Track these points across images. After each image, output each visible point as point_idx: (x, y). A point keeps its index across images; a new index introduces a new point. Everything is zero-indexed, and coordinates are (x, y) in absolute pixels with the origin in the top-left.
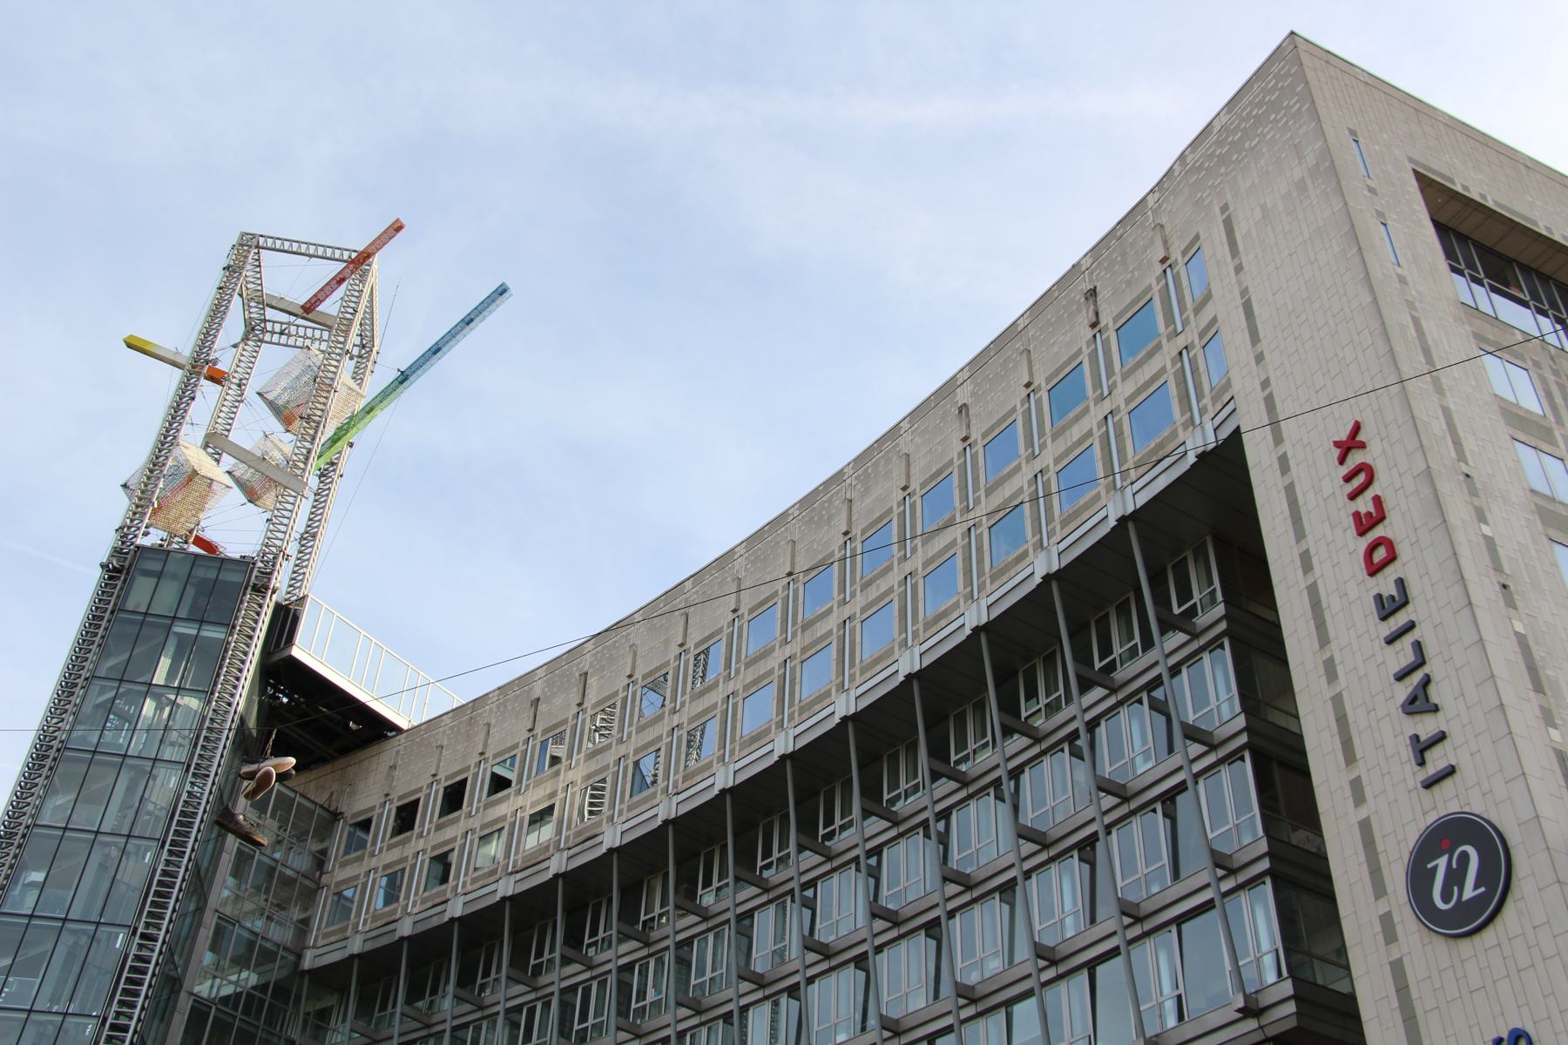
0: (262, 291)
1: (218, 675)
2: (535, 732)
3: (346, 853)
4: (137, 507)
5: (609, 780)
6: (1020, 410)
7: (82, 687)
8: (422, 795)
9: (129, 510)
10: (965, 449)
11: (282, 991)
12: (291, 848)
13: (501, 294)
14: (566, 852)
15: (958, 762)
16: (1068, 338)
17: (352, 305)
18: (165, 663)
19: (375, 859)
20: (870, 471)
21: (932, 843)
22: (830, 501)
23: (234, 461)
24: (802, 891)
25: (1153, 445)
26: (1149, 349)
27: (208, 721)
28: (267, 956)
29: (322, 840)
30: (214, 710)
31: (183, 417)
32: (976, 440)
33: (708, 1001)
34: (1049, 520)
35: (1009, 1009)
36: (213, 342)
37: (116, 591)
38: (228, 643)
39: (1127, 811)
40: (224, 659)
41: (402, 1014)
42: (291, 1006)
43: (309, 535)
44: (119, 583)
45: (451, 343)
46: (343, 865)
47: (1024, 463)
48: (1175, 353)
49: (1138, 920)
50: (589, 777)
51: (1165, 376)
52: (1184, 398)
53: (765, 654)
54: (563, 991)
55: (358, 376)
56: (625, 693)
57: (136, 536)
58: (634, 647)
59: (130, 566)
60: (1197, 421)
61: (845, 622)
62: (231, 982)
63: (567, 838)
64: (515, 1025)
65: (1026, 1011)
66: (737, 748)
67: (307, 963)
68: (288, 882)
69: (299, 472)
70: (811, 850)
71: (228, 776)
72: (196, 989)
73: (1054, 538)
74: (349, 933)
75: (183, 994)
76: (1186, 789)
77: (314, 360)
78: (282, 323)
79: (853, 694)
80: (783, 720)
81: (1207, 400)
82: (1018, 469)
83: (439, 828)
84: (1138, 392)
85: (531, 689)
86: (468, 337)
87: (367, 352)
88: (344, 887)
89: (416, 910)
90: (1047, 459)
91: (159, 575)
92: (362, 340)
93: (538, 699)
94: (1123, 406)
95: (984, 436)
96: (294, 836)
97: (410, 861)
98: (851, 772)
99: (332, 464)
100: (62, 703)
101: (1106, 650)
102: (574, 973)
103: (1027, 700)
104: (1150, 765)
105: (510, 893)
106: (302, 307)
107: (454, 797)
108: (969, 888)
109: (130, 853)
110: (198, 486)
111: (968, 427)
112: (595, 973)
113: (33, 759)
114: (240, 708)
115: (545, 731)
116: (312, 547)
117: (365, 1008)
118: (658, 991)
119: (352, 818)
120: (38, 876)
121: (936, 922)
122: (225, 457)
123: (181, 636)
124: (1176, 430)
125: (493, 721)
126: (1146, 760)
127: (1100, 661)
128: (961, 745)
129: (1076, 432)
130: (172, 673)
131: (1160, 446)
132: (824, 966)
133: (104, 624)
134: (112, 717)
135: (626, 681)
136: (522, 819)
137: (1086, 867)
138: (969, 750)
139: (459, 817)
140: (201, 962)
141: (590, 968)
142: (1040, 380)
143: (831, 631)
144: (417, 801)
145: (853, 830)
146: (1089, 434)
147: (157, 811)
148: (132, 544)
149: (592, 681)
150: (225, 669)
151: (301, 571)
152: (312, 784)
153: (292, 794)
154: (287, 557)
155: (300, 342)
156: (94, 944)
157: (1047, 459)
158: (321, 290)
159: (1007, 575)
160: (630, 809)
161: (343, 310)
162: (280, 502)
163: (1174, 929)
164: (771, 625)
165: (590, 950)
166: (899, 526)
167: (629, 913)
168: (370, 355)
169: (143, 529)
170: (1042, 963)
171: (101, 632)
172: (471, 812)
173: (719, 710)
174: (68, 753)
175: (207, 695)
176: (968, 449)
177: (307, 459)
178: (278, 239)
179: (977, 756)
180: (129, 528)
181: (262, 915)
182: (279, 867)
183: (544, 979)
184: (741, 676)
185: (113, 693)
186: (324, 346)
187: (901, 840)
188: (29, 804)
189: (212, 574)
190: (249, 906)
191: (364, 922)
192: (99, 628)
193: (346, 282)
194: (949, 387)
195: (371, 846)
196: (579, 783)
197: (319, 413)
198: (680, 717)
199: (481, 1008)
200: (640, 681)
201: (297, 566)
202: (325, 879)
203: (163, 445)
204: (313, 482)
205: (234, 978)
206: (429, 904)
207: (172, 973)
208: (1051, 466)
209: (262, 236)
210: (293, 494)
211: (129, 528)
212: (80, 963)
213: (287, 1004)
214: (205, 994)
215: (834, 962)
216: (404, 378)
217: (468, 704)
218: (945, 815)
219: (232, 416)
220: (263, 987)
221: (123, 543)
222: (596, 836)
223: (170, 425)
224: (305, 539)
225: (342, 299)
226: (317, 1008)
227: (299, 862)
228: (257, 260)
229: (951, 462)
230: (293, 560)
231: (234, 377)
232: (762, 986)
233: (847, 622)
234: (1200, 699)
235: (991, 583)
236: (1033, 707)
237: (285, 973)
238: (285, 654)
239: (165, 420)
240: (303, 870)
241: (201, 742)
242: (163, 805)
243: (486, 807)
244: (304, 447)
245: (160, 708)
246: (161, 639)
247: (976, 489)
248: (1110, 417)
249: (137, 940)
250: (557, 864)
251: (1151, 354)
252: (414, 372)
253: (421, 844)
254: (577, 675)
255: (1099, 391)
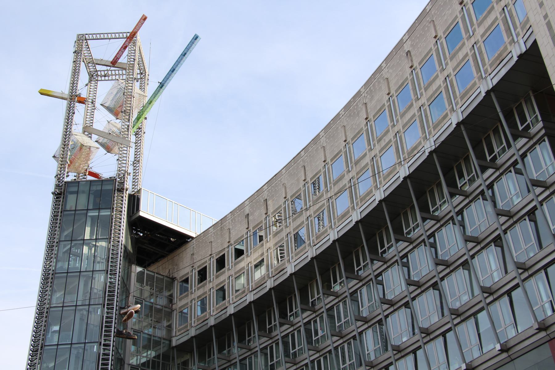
0: (92, 58)
1: (111, 230)
2: (249, 229)
3: (181, 294)
4: (61, 165)
5: (285, 245)
6: (434, 49)
7: (56, 246)
8: (207, 264)
9: (58, 167)
10: (412, 71)
11: (166, 357)
12: (157, 296)
13: (196, 39)
14: (272, 278)
15: (434, 212)
16: (450, 11)
17: (133, 57)
18: (88, 230)
19: (193, 295)
20: (372, 89)
21: (457, 228)
22: (357, 105)
23: (97, 137)
24: (401, 260)
25: (496, 55)
26: (488, 10)
27: (111, 251)
28: (157, 343)
29: (170, 290)
30: (113, 246)
31: (72, 122)
32: (416, 66)
33: (345, 332)
34: (455, 98)
35: (475, 316)
36: (77, 87)
37: (61, 203)
38: (112, 216)
39: (513, 222)
40: (112, 223)
41: (218, 358)
42: (171, 362)
43: (136, 162)
44: (61, 199)
45: (179, 66)
46: (180, 300)
47: (439, 73)
48: (500, 9)
49: (526, 270)
50: (276, 244)
51: (498, 21)
52: (508, 30)
53: (341, 178)
54: (283, 337)
55: (142, 88)
56: (285, 206)
57: (63, 178)
58: (285, 185)
59: (64, 191)
60: (516, 40)
61: (373, 158)
62: (144, 357)
63: (272, 272)
64: (266, 354)
65: (482, 317)
66: (337, 221)
67: (174, 344)
68: (159, 311)
69: (126, 136)
70: (429, 219)
71: (125, 271)
72: (131, 362)
73: (458, 105)
74: (189, 328)
75: (126, 366)
76: (537, 209)
77: (122, 85)
78: (104, 71)
79: (382, 190)
80: (354, 206)
81: (519, 29)
82: (437, 76)
83: (217, 277)
84: (486, 31)
85: (243, 212)
86: (185, 61)
87: (144, 76)
88: (183, 309)
89: (215, 313)
90: (449, 70)
91: (77, 193)
92: (140, 71)
93: (248, 214)
94: (480, 39)
95: (420, 64)
96: (157, 291)
97: (208, 293)
98: (387, 223)
99: (140, 128)
100: (49, 255)
101: (491, 151)
102: (286, 329)
103: (459, 179)
104: (520, 199)
105: (252, 300)
106: (111, 63)
107: (221, 263)
108: (448, 266)
109: (91, 312)
110: (85, 150)
111: (412, 61)
112: (295, 327)
113: (43, 280)
114: (123, 242)
115: (254, 228)
116: (139, 166)
117: (202, 358)
118: (323, 331)
119: (180, 279)
120: (57, 328)
121: (499, 237)
122: (93, 136)
123: (92, 217)
124: (506, 46)
125: (231, 227)
126: (518, 198)
127: (489, 156)
128: (434, 204)
129: (461, 55)
130: (92, 233)
131: (500, 55)
132: (392, 309)
133: (59, 218)
134: (71, 256)
135: (284, 200)
136: (251, 267)
137: (533, 223)
138: (438, 205)
139: (225, 271)
140: (130, 351)
141: (292, 326)
142: (440, 34)
143: (368, 163)
144: (206, 267)
145: (419, 228)
146: (467, 55)
147: (98, 292)
148: (63, 181)
149: (269, 202)
150: (113, 227)
151: (136, 178)
152: (161, 268)
153: (153, 274)
154: (129, 174)
155: (114, 77)
156: (85, 351)
157: (449, 70)
158: (118, 53)
159: (440, 125)
160: (296, 255)
161: (129, 60)
162: (121, 151)
163: (543, 271)
164: (362, 143)
165: (291, 318)
166: (389, 111)
167: (304, 299)
168: (145, 77)
169: (66, 174)
170: (485, 295)
171: (58, 221)
172: (229, 268)
173: (326, 206)
174: (57, 275)
175: (109, 240)
176: (413, 71)
177: (128, 129)
178: (94, 34)
179: (441, 207)
180: (60, 175)
181: (151, 327)
182: (154, 306)
183: (274, 334)
184: (333, 190)
185: (69, 246)
186: (124, 77)
187: (415, 249)
188: (46, 299)
189: (99, 188)
190: (145, 324)
191: (194, 322)
192: (57, 220)
193: (128, 48)
194: (401, 44)
195: (191, 289)
196: (272, 248)
197: (129, 108)
198: (310, 212)
199: (250, 350)
200: (290, 199)
201: (134, 176)
202: (174, 307)
203: (66, 136)
204: (133, 138)
205: (145, 355)
206: (220, 310)
207: (119, 357)
208: (452, 73)
209: (86, 34)
210: (126, 146)
211: (60, 175)
212: (82, 360)
213: (169, 361)
214: (135, 363)
215: (395, 307)
216: (162, 85)
217: (219, 221)
218: (460, 212)
219: (92, 116)
220: (158, 357)
221: (59, 182)
222: (284, 269)
223: (67, 127)
224: (135, 164)
225: (127, 55)
226: (182, 361)
227: (162, 301)
228: (87, 45)
229: (407, 79)
230: (132, 175)
231: (89, 99)
232: (367, 322)
233: (374, 158)
234: (538, 166)
235: (434, 130)
236: (463, 182)
237: (165, 349)
238: (138, 215)
239: (64, 125)
240: (164, 304)
241: (110, 260)
242: (101, 289)
243: (235, 264)
244: (126, 125)
245: (90, 249)
246: (84, 220)
247: (420, 89)
248: (475, 45)
249: (102, 347)
250: (270, 284)
251: (489, 12)
252: (166, 82)
253: (211, 285)
254: (262, 201)
255: (468, 34)
